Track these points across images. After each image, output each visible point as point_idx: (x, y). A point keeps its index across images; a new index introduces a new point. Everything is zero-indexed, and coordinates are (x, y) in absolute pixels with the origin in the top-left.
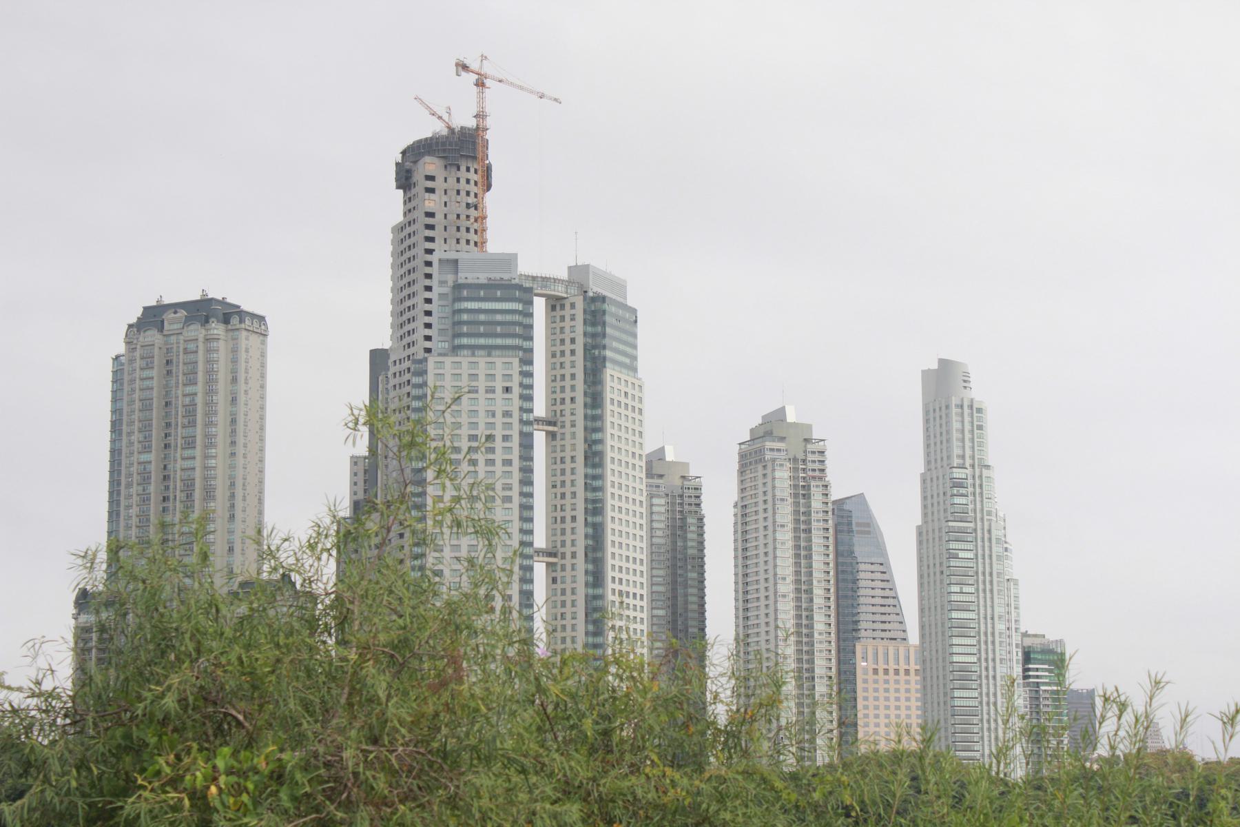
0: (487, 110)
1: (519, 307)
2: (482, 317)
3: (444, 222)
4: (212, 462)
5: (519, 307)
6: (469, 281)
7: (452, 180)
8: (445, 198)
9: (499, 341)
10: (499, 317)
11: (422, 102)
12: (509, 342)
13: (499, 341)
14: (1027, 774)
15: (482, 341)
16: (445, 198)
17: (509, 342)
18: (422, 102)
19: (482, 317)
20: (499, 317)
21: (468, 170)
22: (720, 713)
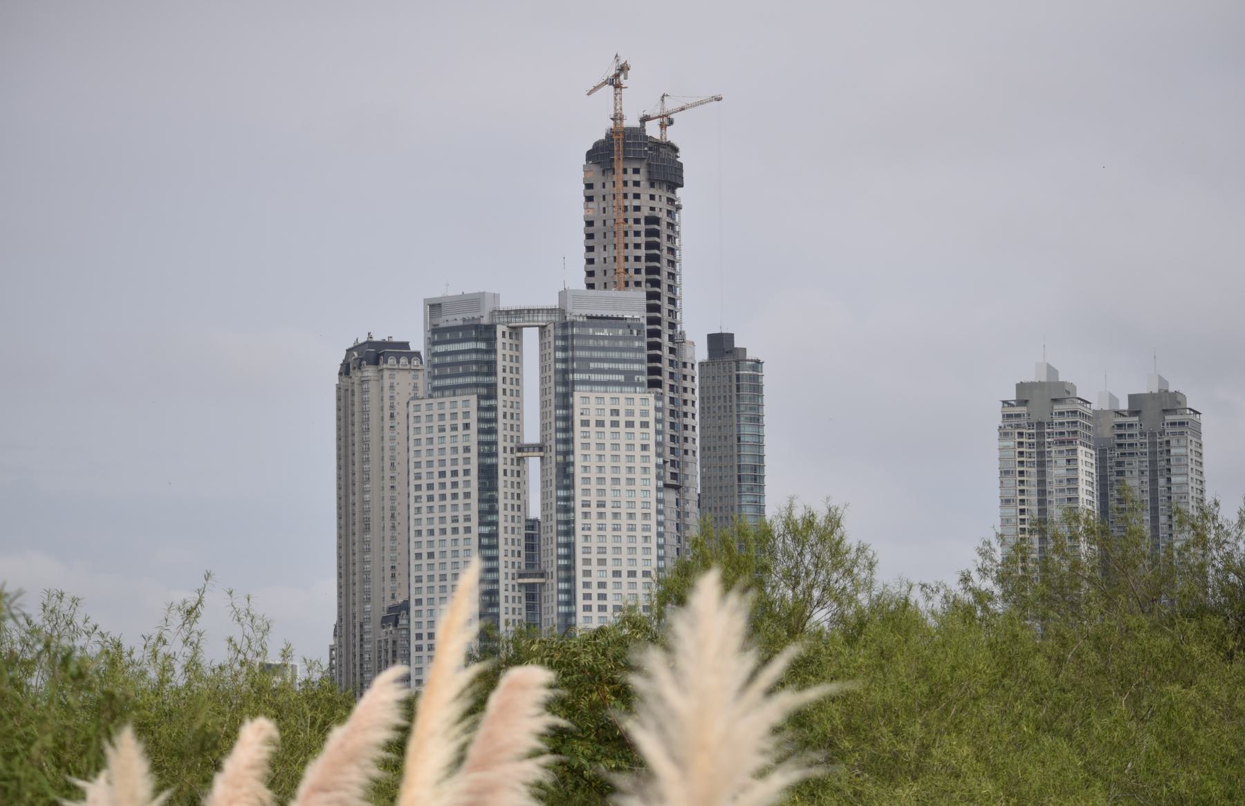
0: (624, 112)
1: (482, 346)
2: (448, 359)
3: (604, 229)
4: (367, 496)
5: (482, 346)
6: (452, 324)
7: (609, 185)
8: (603, 205)
9: (461, 381)
10: (460, 358)
11: (596, 88)
12: (469, 380)
13: (461, 381)
14: (1035, 527)
15: (448, 382)
16: (603, 205)
17: (469, 380)
18: (596, 88)
19: (448, 359)
20: (460, 358)
21: (625, 171)
22: (708, 585)
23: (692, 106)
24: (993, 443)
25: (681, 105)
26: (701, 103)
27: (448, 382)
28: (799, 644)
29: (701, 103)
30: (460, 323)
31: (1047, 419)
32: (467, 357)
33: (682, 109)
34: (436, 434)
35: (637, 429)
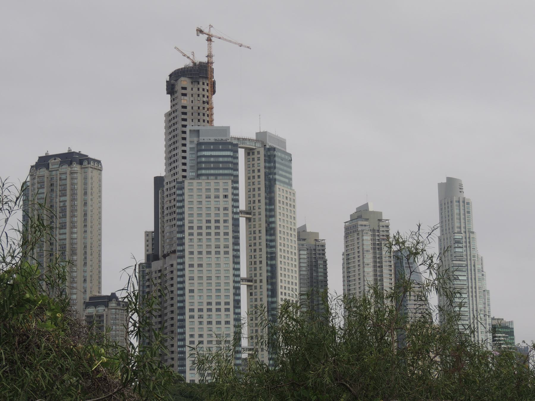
1: (231, 154)
2: (212, 159)
5: (231, 154)
7: (195, 90)
9: (221, 172)
10: (221, 159)
12: (226, 172)
13: (221, 172)
15: (212, 172)
17: (226, 172)
19: (212, 159)
20: (221, 159)
21: (203, 84)
23: (225, 40)
24: (341, 257)
25: (220, 36)
26: (230, 41)
27: (212, 172)
28: (294, 299)
29: (230, 41)
30: (213, 141)
31: (376, 228)
32: (226, 159)
33: (219, 38)
34: (204, 199)
35: (196, 263)
